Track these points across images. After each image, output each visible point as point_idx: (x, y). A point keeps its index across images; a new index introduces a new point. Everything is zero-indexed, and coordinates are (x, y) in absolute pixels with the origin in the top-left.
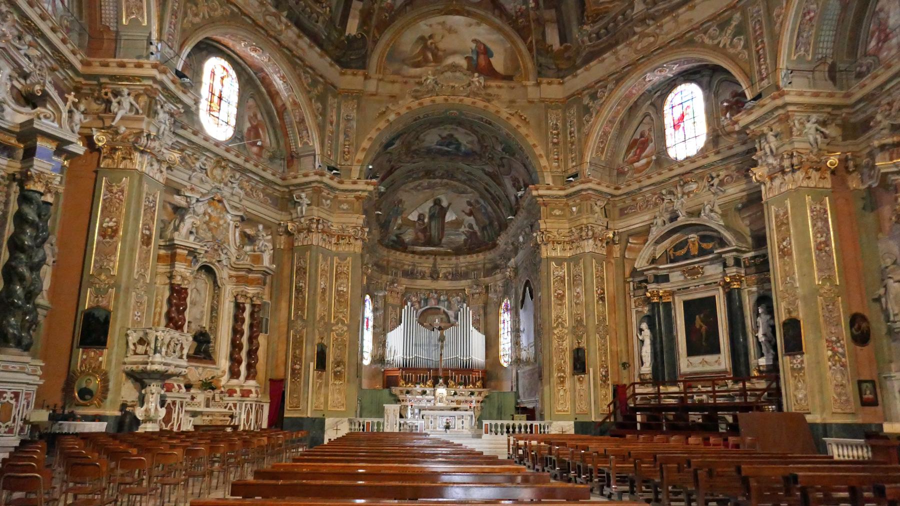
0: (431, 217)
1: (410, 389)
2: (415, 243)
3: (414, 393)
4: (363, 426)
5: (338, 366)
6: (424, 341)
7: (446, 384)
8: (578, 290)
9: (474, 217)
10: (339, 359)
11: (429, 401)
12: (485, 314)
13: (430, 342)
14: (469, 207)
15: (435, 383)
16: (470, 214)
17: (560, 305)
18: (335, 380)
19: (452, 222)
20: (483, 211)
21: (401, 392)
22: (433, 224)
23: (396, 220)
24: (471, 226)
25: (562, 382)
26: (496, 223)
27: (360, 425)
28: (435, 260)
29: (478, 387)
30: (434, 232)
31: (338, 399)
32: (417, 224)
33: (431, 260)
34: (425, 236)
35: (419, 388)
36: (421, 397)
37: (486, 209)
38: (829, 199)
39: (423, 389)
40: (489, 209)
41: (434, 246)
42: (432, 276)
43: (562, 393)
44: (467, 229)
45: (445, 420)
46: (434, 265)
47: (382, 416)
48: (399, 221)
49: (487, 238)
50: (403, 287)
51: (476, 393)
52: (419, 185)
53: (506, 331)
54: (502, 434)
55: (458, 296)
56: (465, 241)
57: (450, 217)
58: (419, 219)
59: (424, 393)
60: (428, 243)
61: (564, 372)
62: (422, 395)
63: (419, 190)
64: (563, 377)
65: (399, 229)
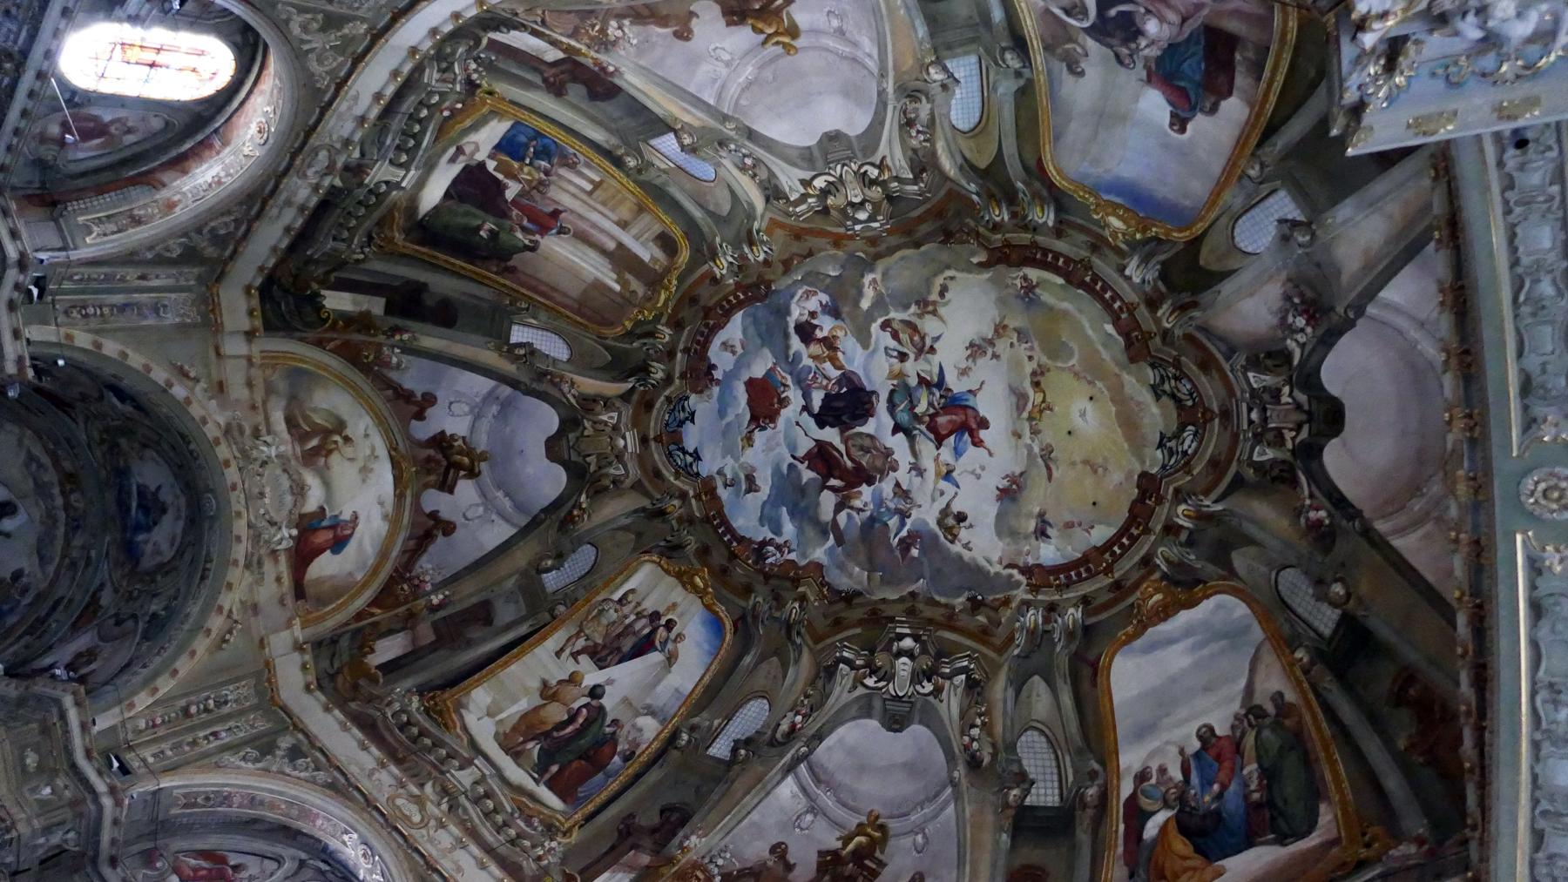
52: (40, 466)
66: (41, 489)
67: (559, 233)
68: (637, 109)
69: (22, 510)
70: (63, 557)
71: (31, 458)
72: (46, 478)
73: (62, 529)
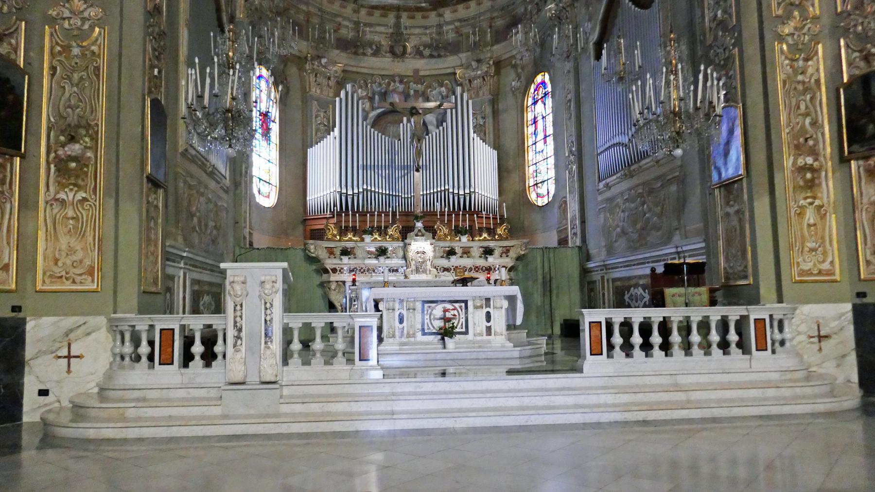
1: (349, 245)
3: (358, 252)
4: (151, 343)
5: (72, 139)
6: (382, 158)
7: (430, 230)
10: (73, 119)
11: (394, 270)
12: (495, 113)
13: (393, 161)
15: (406, 232)
18: (62, 186)
21: (331, 252)
25: (811, 185)
27: (136, 342)
28: (398, 17)
29: (501, 238)
31: (71, 251)
33: (391, 19)
35: (370, 243)
36: (374, 262)
39: (379, 244)
42: (392, 52)
43: (810, 216)
45: (438, 311)
46: (397, 25)
47: (218, 308)
50: (339, 67)
51: (497, 253)
53: (541, 136)
54: (708, 353)
55: (441, 85)
59: (382, 252)
61: (814, 152)
62: (377, 258)
64: (811, 169)
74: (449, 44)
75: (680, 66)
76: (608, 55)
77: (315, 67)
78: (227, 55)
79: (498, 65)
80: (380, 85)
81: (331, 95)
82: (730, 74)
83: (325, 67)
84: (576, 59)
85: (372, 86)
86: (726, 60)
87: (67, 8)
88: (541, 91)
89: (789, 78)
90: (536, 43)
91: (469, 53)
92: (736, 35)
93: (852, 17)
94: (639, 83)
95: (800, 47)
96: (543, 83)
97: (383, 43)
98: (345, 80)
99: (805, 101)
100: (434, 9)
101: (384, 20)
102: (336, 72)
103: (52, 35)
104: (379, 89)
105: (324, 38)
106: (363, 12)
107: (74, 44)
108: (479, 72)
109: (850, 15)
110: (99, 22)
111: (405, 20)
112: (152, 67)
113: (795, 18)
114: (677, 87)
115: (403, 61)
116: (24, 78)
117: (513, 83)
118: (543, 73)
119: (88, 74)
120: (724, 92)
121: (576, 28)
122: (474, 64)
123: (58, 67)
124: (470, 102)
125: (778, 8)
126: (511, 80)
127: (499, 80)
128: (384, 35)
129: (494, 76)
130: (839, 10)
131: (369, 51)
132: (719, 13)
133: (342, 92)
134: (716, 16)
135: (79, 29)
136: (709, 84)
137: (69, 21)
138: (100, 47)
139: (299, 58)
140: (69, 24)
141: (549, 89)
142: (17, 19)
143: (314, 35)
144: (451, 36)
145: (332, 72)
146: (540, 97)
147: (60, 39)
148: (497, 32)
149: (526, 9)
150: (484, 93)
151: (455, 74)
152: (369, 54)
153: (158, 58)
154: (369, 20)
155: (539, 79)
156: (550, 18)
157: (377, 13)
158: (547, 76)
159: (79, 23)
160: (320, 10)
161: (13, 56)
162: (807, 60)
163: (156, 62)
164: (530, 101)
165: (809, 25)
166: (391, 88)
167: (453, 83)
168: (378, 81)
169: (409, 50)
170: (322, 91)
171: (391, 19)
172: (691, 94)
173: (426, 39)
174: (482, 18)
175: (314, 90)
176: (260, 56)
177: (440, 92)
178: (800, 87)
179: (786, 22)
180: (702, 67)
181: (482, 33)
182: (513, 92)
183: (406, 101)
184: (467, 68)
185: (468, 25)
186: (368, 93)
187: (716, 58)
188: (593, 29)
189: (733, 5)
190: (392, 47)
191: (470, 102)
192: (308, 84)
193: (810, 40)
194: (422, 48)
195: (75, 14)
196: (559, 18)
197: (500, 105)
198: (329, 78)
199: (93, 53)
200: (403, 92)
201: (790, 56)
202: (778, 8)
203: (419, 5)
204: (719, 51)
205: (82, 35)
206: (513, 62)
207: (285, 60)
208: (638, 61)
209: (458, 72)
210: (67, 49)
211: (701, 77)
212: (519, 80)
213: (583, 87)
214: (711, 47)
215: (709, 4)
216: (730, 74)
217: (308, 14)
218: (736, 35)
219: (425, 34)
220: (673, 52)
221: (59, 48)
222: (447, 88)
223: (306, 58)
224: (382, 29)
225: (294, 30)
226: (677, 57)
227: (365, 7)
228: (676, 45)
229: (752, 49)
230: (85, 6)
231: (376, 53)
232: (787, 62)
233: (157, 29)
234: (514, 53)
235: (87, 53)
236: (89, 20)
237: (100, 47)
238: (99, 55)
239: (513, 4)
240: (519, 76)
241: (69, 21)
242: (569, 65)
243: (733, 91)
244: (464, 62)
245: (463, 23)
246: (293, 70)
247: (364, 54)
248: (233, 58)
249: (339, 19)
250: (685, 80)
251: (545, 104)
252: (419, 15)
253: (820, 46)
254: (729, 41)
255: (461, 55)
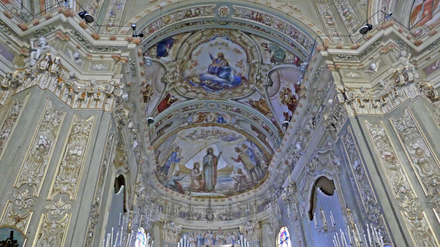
0: (205, 166)
2: (191, 189)
8: (416, 145)
9: (243, 162)
14: (238, 154)
16: (239, 159)
17: (395, 169)
19: (222, 170)
20: (251, 154)
22: (207, 172)
23: (174, 166)
24: (240, 172)
26: (263, 162)
28: (210, 201)
30: (208, 180)
32: (193, 172)
33: (206, 202)
34: (200, 183)
37: (252, 151)
38: (425, 212)
40: (256, 150)
41: (209, 191)
42: (207, 218)
44: (237, 175)
46: (210, 205)
48: (177, 168)
49: (255, 178)
50: (180, 227)
52: (194, 133)
55: (232, 234)
56: (236, 185)
57: (221, 165)
58: (195, 168)
60: (203, 189)
63: (193, 139)
65: (177, 175)
66: (203, 136)
67: (378, 244)
68: (379, 30)
69: (212, 146)
70: (234, 128)
71: (190, 136)
72: (199, 133)
73: (222, 128)
74: (235, 213)
75: (356, 225)
76: (317, 218)
77: (168, 227)
78: (128, 225)
79: (260, 223)
80: (201, 235)
81: (175, 241)
82: (382, 228)
83: (173, 227)
84: (300, 220)
85: (196, 236)
86: (378, 220)
87: (55, 205)
88: (284, 237)
89: (414, 229)
90: (278, 212)
91: (245, 218)
92: (380, 208)
93: (434, 198)
94: (337, 234)
95: (414, 213)
96: (285, 232)
97: (202, 213)
98: (183, 233)
99: (426, 241)
100: (227, 197)
101: (202, 203)
102: (179, 229)
103: (44, 218)
104: (200, 237)
105: (174, 212)
106: (193, 199)
107: (54, 222)
108: (251, 227)
109: (433, 197)
110: (69, 211)
111: (213, 202)
112: (89, 232)
113: (406, 199)
114: (357, 236)
115: (212, 222)
116: (25, 240)
117: (269, 232)
118: (284, 227)
119: (57, 238)
120: (382, 237)
121: (298, 205)
122: (248, 223)
123: (43, 234)
124: (248, 243)
125: (397, 195)
126: (267, 229)
127: (262, 232)
128: (203, 210)
129: (259, 229)
130: (427, 195)
131: (195, 218)
132: (368, 198)
133: (181, 239)
134: (367, 199)
135: (58, 215)
136: (373, 234)
137: (54, 211)
138: (66, 223)
139: (160, 222)
140: (54, 213)
141: (288, 235)
142: (30, 211)
143: (168, 211)
144: (236, 210)
145: (176, 229)
146: (284, 240)
147: (48, 220)
148: (258, 207)
149: (271, 196)
150: (254, 238)
151: (239, 228)
152: (195, 219)
153: (93, 228)
154: (196, 203)
155: (282, 230)
156: (284, 200)
157: (200, 199)
158: (286, 229)
159: (59, 211)
160: (172, 199)
161: (22, 229)
162: (420, 219)
163: (92, 230)
164: (279, 242)
165: (414, 202)
166: (206, 236)
167: (238, 233)
168: (199, 233)
169: (215, 217)
170: (171, 238)
171: (206, 202)
172: (365, 239)
173: (224, 211)
174: (250, 200)
175: (167, 239)
176: (142, 223)
177: (232, 238)
178: (421, 234)
179: (402, 201)
180: (368, 225)
181: (251, 208)
182: (270, 237)
183: (214, 244)
184: (244, 225)
185: (244, 204)
186: (194, 240)
187: (373, 219)
188: (306, 205)
189: (374, 194)
190: (207, 216)
191: (248, 243)
192: (164, 235)
193: (418, 210)
194: (221, 216)
195: (58, 208)
196: (289, 200)
197: (263, 244)
198: (175, 232)
199: (62, 226)
200: (212, 239)
201: (410, 218)
202: (397, 195)
203: (220, 195)
204: (373, 216)
205: (59, 217)
206: (268, 221)
207: (153, 224)
208: (333, 222)
209: (240, 227)
210: (50, 224)
211: (368, 230)
212: (272, 230)
213: (306, 234)
214: (368, 214)
215: (362, 193)
216: (382, 228)
217: (166, 202)
218: (380, 208)
219: (223, 209)
220: (350, 217)
221: (46, 224)
222: (235, 236)
223: (164, 222)
224: (202, 207)
225: (159, 209)
226: (353, 220)
227: (194, 197)
228: (351, 214)
229: (389, 214)
230: (63, 204)
231: (199, 219)
232: (410, 221)
233: (95, 213)
234: (268, 217)
235: (59, 226)
236: (64, 210)
237: (66, 223)
238: (65, 227)
239: (265, 193)
240: (272, 229)
241: (54, 211)
242: (297, 223)
243: (387, 236)
244: (243, 222)
245: (241, 203)
246: (157, 228)
247: (193, 219)
248: (130, 228)
249: (181, 203)
250: (360, 232)
251: (287, 243)
252: (220, 200)
253: (424, 212)
254: (377, 211)
255: (241, 219)
